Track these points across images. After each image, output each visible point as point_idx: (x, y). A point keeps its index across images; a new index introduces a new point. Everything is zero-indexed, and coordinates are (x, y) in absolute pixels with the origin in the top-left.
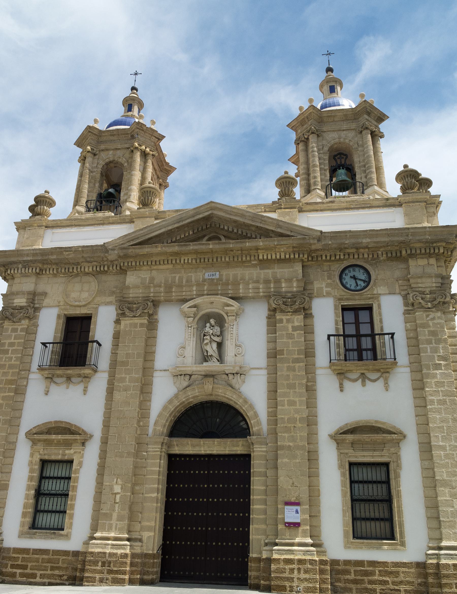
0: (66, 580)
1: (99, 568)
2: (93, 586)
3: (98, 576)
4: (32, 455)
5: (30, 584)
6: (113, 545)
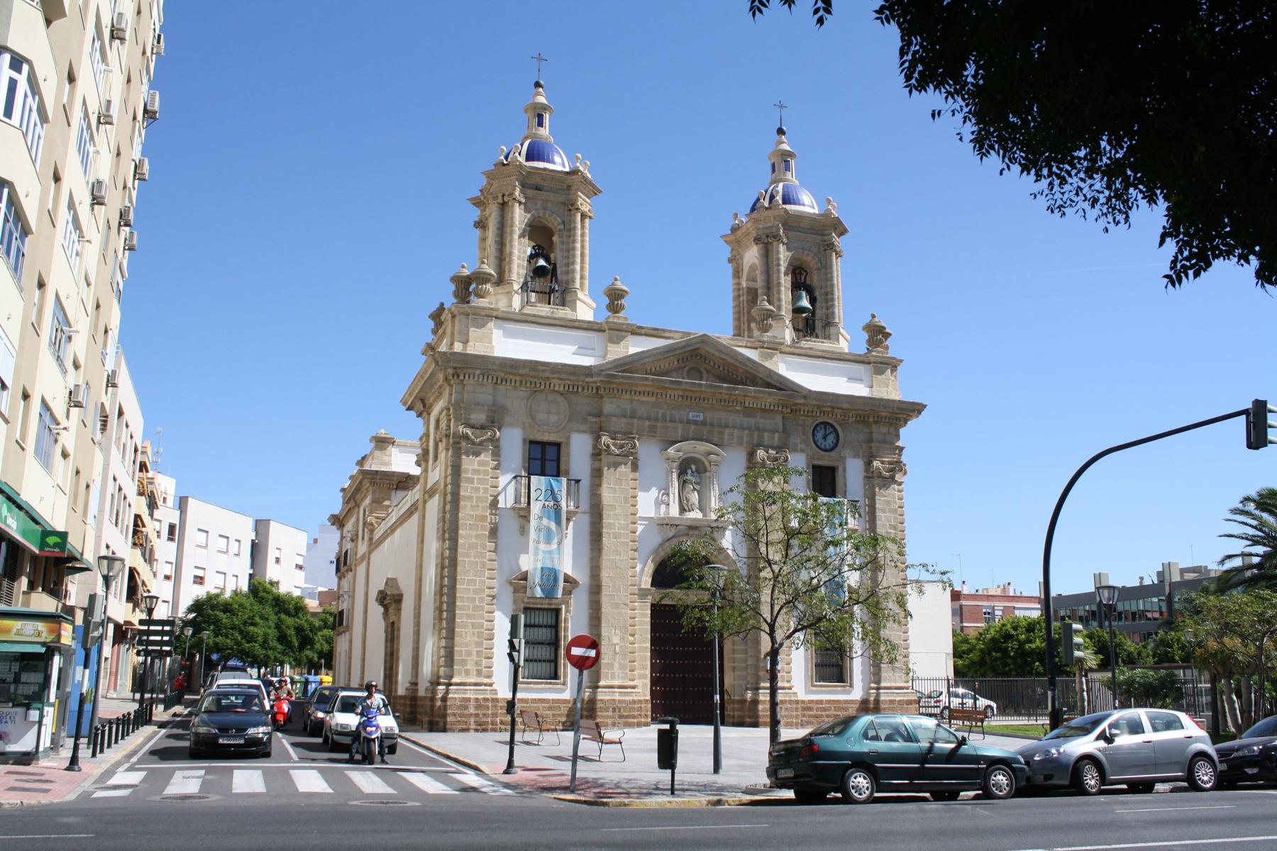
3: (609, 721)
4: (515, 602)
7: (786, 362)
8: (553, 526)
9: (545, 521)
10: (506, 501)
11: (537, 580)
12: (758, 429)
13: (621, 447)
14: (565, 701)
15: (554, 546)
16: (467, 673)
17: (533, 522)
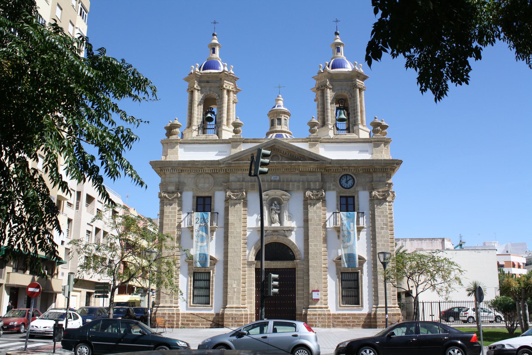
3: (230, 324)
4: (189, 270)
7: (324, 147)
8: (204, 234)
9: (201, 232)
10: (330, 225)
11: (198, 259)
12: (308, 181)
13: (237, 195)
14: (212, 314)
15: (205, 244)
16: (166, 302)
17: (195, 234)
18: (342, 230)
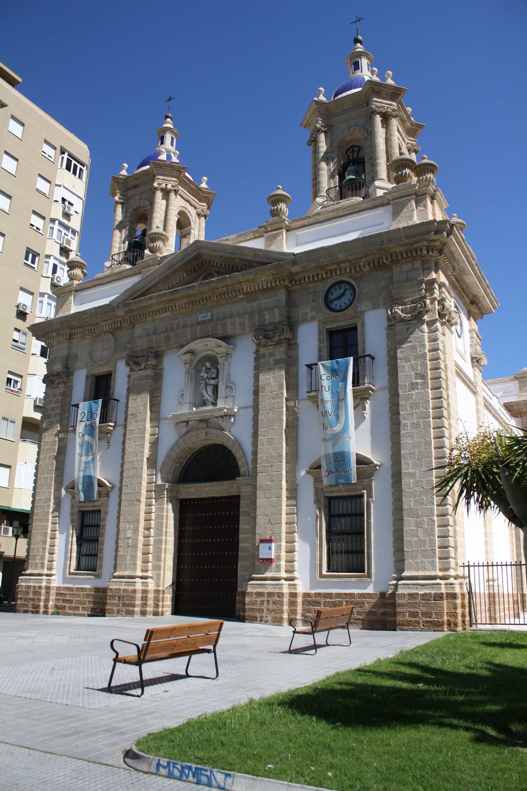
0: (99, 612)
1: (116, 602)
2: (112, 616)
3: (115, 609)
5: (75, 615)
6: (126, 582)
11: (80, 487)
18: (322, 400)
